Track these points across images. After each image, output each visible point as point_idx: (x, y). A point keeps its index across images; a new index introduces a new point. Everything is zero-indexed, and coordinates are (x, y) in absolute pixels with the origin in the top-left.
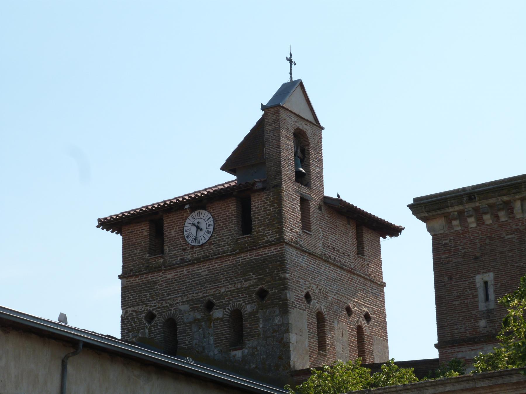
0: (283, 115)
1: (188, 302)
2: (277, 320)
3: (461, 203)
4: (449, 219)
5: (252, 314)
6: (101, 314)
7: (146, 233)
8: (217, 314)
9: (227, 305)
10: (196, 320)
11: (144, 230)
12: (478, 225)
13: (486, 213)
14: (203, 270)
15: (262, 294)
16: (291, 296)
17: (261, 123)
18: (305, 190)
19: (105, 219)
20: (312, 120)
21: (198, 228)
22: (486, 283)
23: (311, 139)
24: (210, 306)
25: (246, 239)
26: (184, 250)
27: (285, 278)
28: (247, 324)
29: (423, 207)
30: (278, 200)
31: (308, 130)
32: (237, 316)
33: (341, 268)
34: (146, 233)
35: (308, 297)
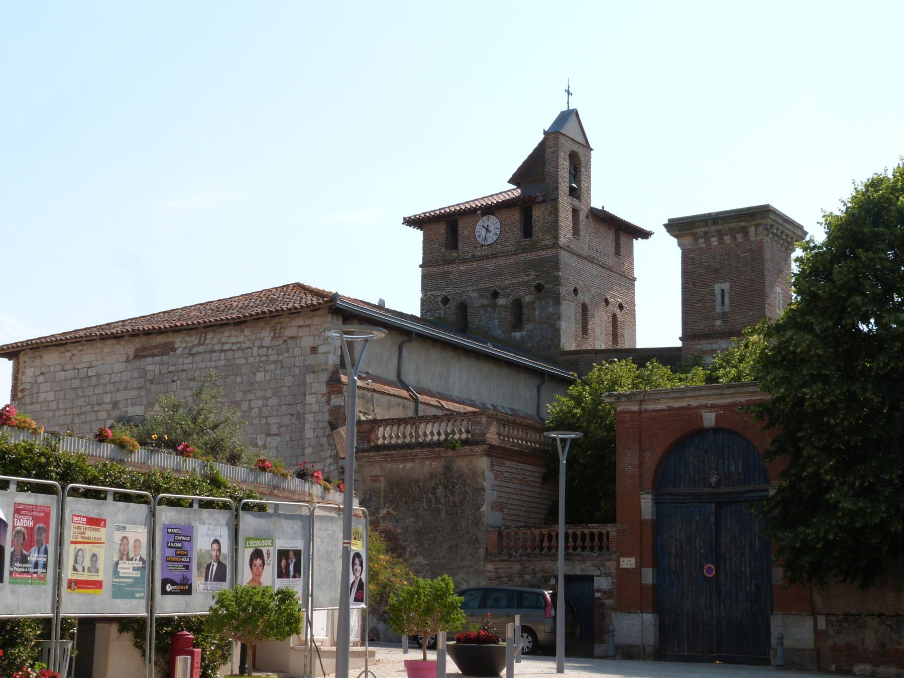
0: (562, 140)
1: (477, 290)
2: (551, 310)
3: (706, 226)
4: (696, 237)
5: (531, 303)
6: (405, 296)
7: (444, 231)
8: (502, 301)
9: (510, 295)
10: (483, 306)
11: (442, 229)
12: (719, 244)
13: (726, 235)
14: (490, 265)
15: (539, 288)
16: (564, 290)
17: (542, 146)
18: (576, 202)
19: (410, 218)
20: (584, 143)
21: (487, 230)
22: (723, 291)
23: (582, 159)
24: (495, 295)
25: (527, 241)
26: (475, 247)
27: (559, 276)
28: (525, 311)
29: (676, 227)
30: (555, 211)
31: (580, 151)
32: (518, 305)
33: (602, 267)
34: (443, 231)
35: (575, 291)
